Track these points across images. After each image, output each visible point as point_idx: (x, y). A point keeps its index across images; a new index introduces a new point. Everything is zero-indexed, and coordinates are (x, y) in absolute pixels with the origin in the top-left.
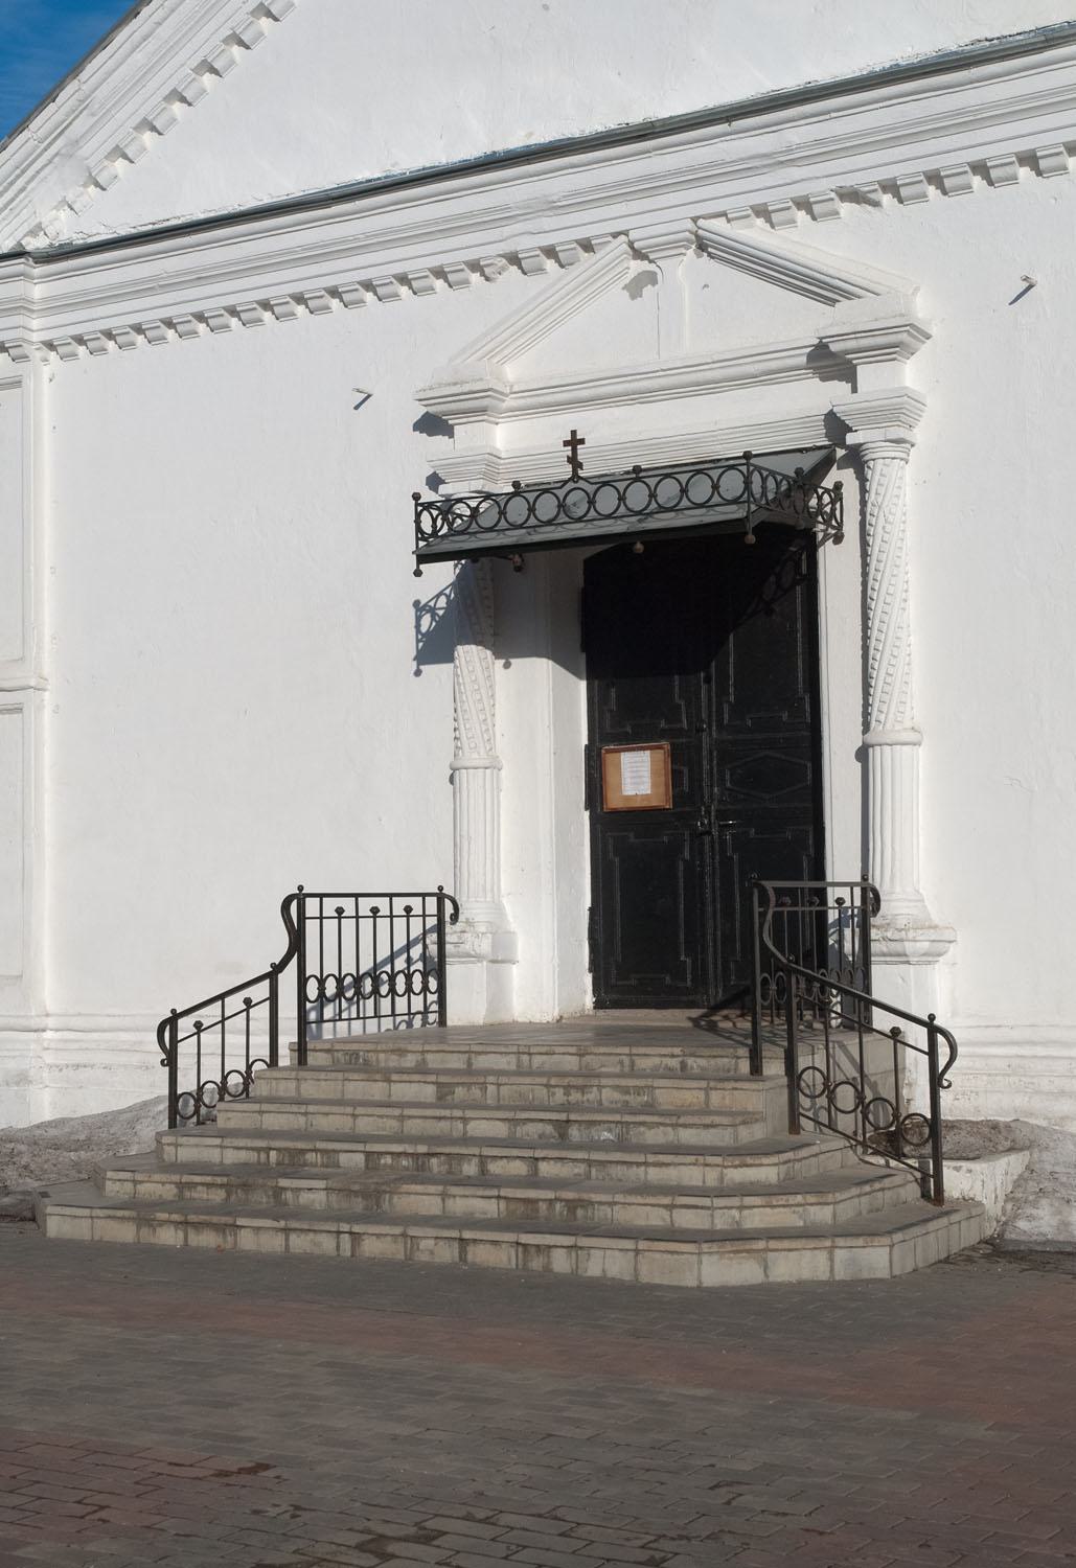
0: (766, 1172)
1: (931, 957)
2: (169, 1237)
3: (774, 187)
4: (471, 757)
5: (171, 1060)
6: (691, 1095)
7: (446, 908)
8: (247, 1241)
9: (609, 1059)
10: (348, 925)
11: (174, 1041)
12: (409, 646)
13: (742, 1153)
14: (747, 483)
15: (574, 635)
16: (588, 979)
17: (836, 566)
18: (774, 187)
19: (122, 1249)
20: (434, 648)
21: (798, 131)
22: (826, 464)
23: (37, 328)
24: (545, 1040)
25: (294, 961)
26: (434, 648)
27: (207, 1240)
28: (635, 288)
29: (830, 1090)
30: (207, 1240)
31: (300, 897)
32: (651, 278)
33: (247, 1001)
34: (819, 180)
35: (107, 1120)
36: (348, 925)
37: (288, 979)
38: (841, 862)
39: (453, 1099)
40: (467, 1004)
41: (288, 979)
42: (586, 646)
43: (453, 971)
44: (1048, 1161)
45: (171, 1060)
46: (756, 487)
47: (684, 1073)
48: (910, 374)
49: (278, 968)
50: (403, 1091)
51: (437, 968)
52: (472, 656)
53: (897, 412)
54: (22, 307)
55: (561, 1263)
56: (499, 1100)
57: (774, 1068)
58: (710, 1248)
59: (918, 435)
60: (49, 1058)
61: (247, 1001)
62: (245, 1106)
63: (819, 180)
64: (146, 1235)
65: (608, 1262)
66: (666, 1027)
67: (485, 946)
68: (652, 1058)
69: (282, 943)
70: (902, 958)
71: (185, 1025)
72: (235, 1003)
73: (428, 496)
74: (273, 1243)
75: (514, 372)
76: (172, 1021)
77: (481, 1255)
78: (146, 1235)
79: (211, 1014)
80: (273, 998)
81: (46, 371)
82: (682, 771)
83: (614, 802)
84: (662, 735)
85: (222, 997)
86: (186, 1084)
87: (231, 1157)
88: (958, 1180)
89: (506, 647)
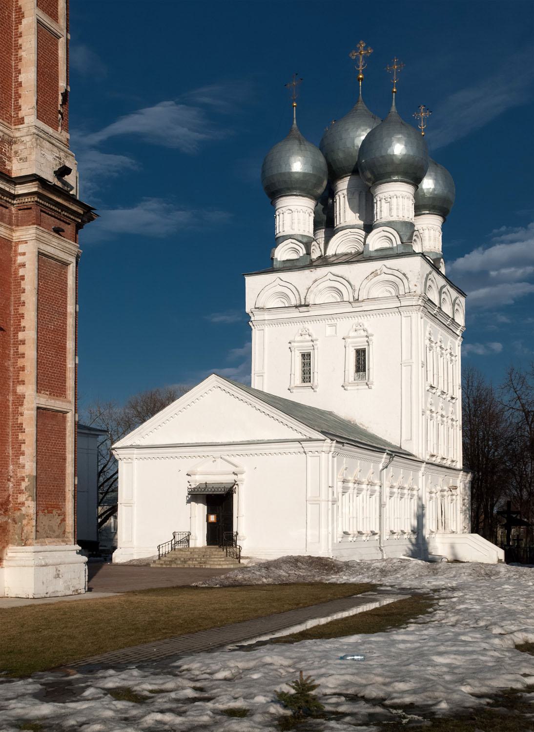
0: (223, 559)
1: (243, 540)
2: (164, 566)
3: (230, 453)
4: (193, 516)
6: (216, 553)
7: (190, 534)
8: (173, 566)
9: (208, 550)
12: (186, 502)
13: (222, 558)
15: (205, 501)
16: (206, 542)
17: (235, 496)
18: (230, 453)
19: (220, 569)
20: (189, 502)
21: (232, 447)
22: (234, 485)
23: (135, 456)
26: (189, 502)
27: (169, 566)
28: (213, 462)
29: (230, 552)
30: (169, 566)
32: (215, 461)
34: (235, 453)
35: (150, 558)
38: (235, 530)
40: (192, 545)
41: (174, 541)
42: (207, 502)
43: (190, 541)
44: (252, 560)
45: (159, 550)
47: (216, 551)
48: (317, 342)
50: (186, 553)
51: (188, 541)
52: (193, 503)
53: (241, 481)
54: (133, 454)
55: (204, 567)
57: (225, 550)
59: (244, 483)
60: (136, 552)
62: (335, 487)
63: (235, 453)
64: (162, 566)
65: (208, 566)
67: (194, 538)
68: (213, 550)
70: (240, 540)
71: (161, 546)
72: (167, 544)
73: (190, 487)
74: (176, 566)
75: (199, 469)
77: (196, 566)
78: (162, 566)
81: (135, 461)
82: (218, 518)
83: (210, 521)
84: (216, 514)
86: (161, 553)
87: (169, 559)
88: (242, 561)
89: (197, 502)
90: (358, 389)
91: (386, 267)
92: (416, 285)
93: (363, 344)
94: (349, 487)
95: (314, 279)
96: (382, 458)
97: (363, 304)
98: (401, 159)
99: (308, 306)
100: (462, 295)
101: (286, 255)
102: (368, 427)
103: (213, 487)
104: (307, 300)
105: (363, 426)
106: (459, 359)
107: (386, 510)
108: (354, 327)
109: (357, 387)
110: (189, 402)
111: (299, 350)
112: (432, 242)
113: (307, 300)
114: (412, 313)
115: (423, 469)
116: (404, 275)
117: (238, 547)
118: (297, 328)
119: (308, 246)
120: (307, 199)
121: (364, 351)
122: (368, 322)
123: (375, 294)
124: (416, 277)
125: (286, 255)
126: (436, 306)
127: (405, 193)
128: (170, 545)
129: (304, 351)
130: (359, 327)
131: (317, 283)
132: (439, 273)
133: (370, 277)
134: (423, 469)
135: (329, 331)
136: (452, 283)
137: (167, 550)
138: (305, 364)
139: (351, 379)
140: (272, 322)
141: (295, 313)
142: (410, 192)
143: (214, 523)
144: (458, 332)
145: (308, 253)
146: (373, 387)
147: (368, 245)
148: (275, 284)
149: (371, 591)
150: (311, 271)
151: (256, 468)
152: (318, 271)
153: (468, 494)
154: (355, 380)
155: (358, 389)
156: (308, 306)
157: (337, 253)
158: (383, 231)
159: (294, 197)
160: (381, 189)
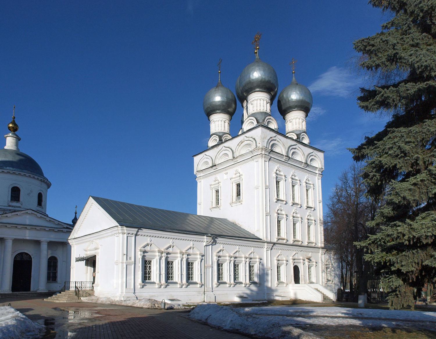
72: (88, 282)
90: (237, 205)
92: (259, 143)
93: (238, 181)
94: (257, 261)
96: (265, 245)
97: (237, 159)
98: (268, 80)
99: (215, 166)
100: (319, 151)
101: (213, 143)
102: (241, 225)
105: (239, 225)
107: (175, 263)
108: (235, 172)
109: (236, 204)
110: (88, 210)
111: (214, 189)
112: (297, 125)
113: (215, 163)
114: (259, 159)
115: (266, 246)
116: (254, 139)
118: (213, 178)
120: (222, 114)
122: (240, 168)
123: (243, 152)
124: (260, 139)
125: (213, 143)
126: (284, 155)
127: (260, 97)
129: (217, 189)
130: (237, 172)
133: (240, 144)
134: (266, 246)
135: (225, 177)
139: (234, 200)
140: (205, 176)
141: (212, 170)
142: (266, 97)
143: (359, 295)
144: (317, 172)
146: (243, 203)
147: (243, 128)
148: (204, 158)
149: (99, 307)
150: (217, 148)
152: (219, 147)
154: (236, 200)
155: (237, 205)
156: (215, 166)
158: (250, 119)
159: (218, 114)
160: (249, 98)
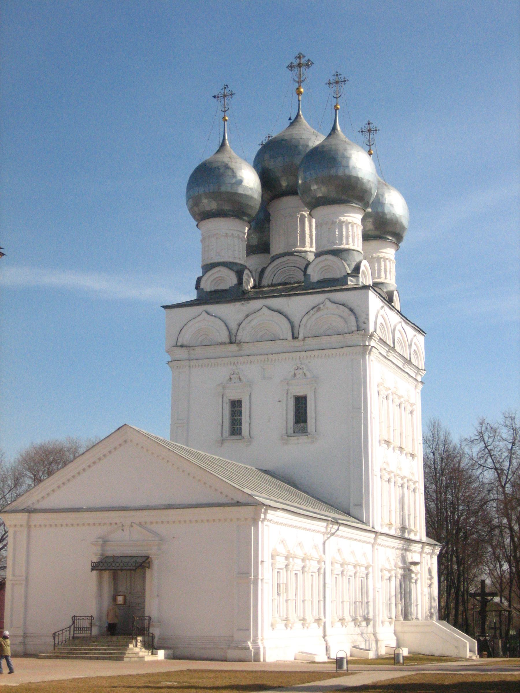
5: (54, 639)
10: (80, 620)
11: (55, 636)
14: (136, 564)
24: (61, 653)
25: (73, 626)
31: (74, 616)
33: (66, 631)
36: (80, 620)
37: (72, 628)
39: (404, 544)
41: (72, 628)
45: (54, 639)
46: (137, 565)
49: (70, 627)
56: (209, 186)
58: (196, 682)
61: (66, 631)
66: (504, 671)
69: (71, 622)
71: (57, 634)
72: (64, 631)
76: (55, 633)
79: (61, 632)
80: (70, 630)
85: (62, 630)
91: (330, 301)
95: (246, 313)
103: (105, 562)
104: (244, 344)
106: (420, 529)
117: (151, 635)
119: (240, 274)
121: (305, 398)
128: (68, 633)
131: (249, 318)
132: (393, 308)
133: (312, 312)
136: (407, 320)
137: (64, 638)
138: (235, 413)
145: (240, 282)
151: (337, 544)
153: (459, 680)
157: (274, 283)
